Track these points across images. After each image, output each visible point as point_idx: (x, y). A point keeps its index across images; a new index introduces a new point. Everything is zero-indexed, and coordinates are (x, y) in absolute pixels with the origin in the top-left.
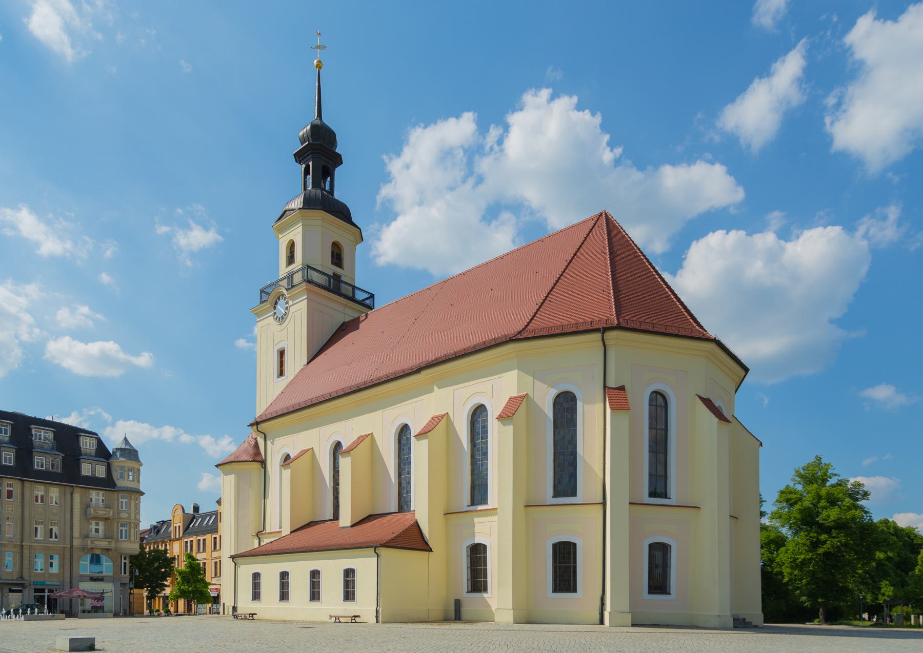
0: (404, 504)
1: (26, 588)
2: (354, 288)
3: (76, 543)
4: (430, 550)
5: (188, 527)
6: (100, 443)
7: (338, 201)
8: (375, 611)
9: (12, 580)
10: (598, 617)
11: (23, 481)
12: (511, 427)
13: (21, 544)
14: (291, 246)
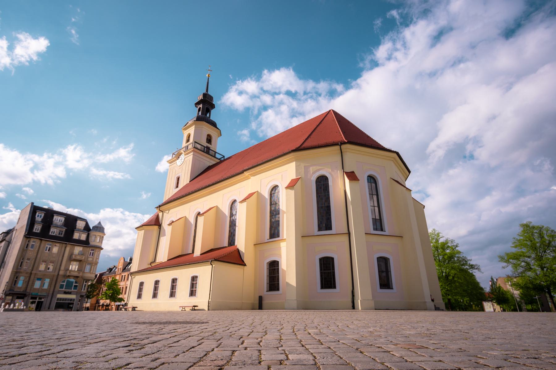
0: (232, 241)
1: (26, 296)
2: (216, 152)
3: (61, 273)
4: (245, 265)
5: (125, 268)
6: (87, 225)
7: (211, 120)
8: (208, 302)
9: (20, 292)
10: (351, 304)
11: (41, 240)
12: (294, 191)
13: (31, 272)
14: (189, 136)
